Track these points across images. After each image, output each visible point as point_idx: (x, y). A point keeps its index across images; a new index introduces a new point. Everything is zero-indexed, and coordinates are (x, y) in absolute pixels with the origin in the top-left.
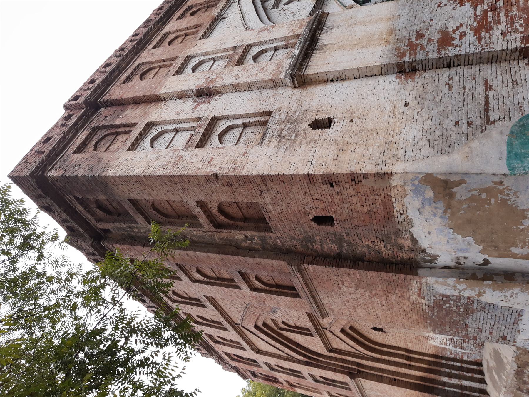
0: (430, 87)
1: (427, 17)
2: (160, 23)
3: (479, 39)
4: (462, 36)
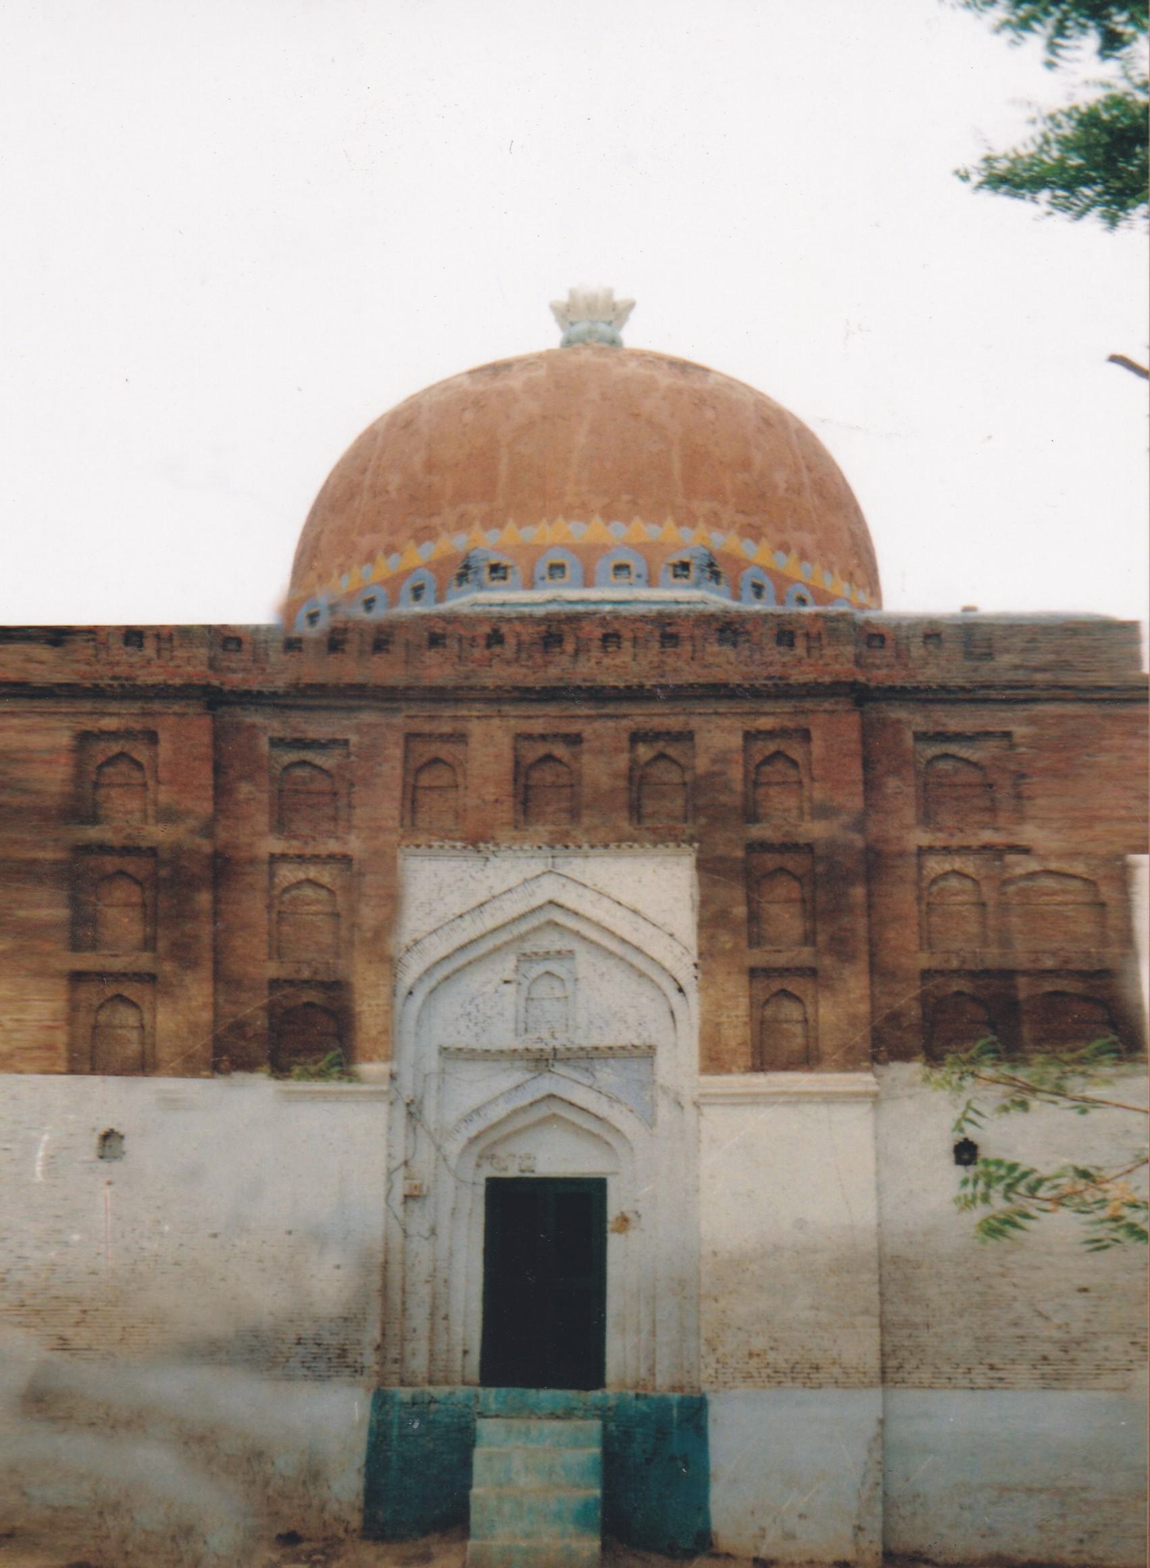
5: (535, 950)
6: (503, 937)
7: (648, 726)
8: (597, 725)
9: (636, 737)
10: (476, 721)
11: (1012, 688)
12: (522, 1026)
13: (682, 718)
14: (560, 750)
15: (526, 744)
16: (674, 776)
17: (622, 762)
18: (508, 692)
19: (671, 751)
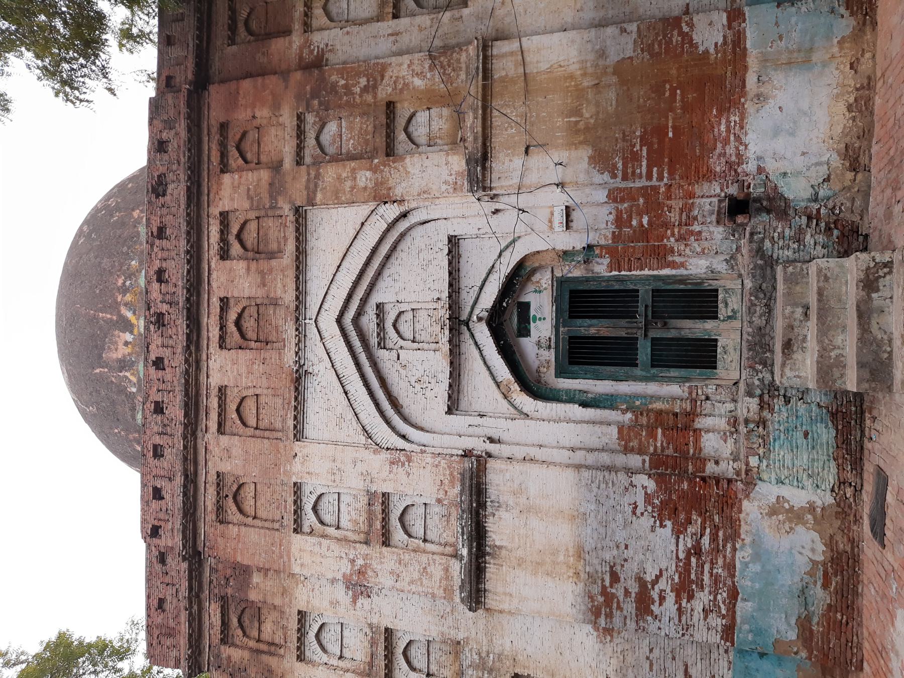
0: (630, 659)
1: (620, 536)
2: (193, 348)
3: (679, 610)
4: (662, 599)
5: (375, 334)
6: (363, 358)
7: (216, 247)
8: (214, 285)
9: (224, 255)
10: (210, 380)
11: (196, 383)
12: (434, 346)
13: (212, 221)
14: (232, 316)
15: (228, 340)
16: (252, 226)
17: (240, 266)
18: (190, 355)
19: (235, 230)
